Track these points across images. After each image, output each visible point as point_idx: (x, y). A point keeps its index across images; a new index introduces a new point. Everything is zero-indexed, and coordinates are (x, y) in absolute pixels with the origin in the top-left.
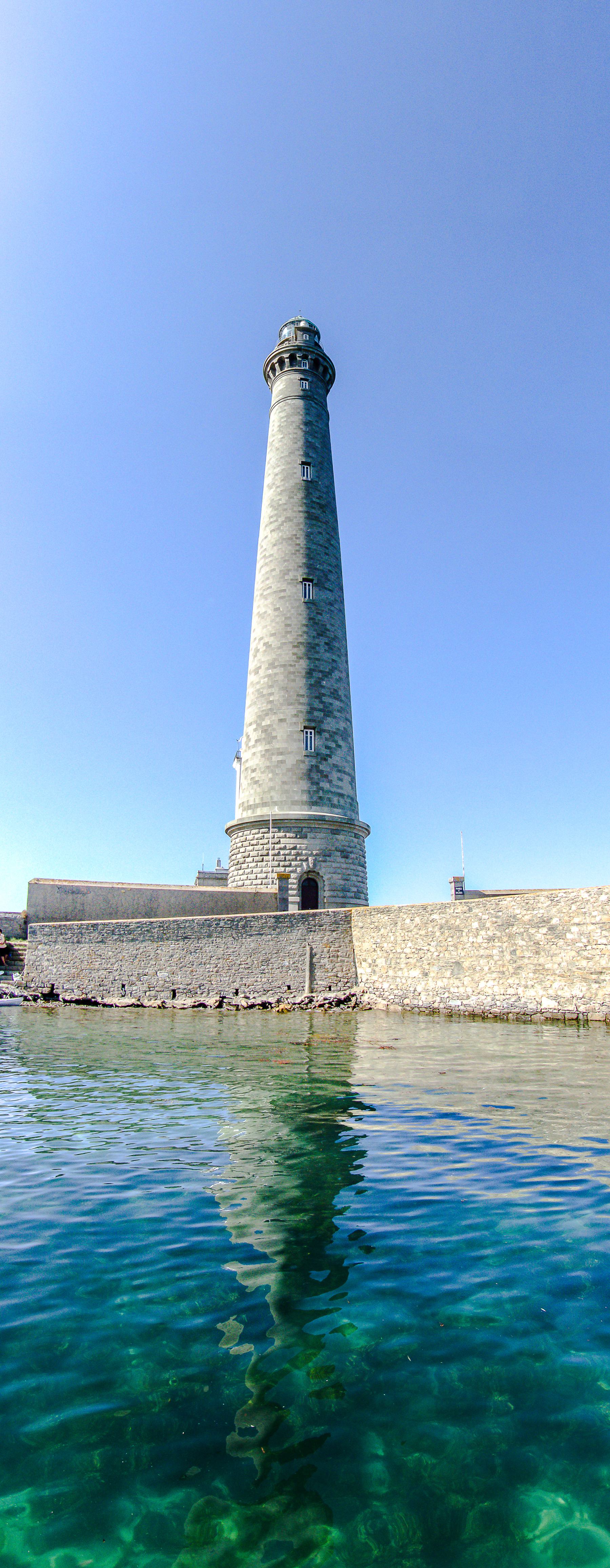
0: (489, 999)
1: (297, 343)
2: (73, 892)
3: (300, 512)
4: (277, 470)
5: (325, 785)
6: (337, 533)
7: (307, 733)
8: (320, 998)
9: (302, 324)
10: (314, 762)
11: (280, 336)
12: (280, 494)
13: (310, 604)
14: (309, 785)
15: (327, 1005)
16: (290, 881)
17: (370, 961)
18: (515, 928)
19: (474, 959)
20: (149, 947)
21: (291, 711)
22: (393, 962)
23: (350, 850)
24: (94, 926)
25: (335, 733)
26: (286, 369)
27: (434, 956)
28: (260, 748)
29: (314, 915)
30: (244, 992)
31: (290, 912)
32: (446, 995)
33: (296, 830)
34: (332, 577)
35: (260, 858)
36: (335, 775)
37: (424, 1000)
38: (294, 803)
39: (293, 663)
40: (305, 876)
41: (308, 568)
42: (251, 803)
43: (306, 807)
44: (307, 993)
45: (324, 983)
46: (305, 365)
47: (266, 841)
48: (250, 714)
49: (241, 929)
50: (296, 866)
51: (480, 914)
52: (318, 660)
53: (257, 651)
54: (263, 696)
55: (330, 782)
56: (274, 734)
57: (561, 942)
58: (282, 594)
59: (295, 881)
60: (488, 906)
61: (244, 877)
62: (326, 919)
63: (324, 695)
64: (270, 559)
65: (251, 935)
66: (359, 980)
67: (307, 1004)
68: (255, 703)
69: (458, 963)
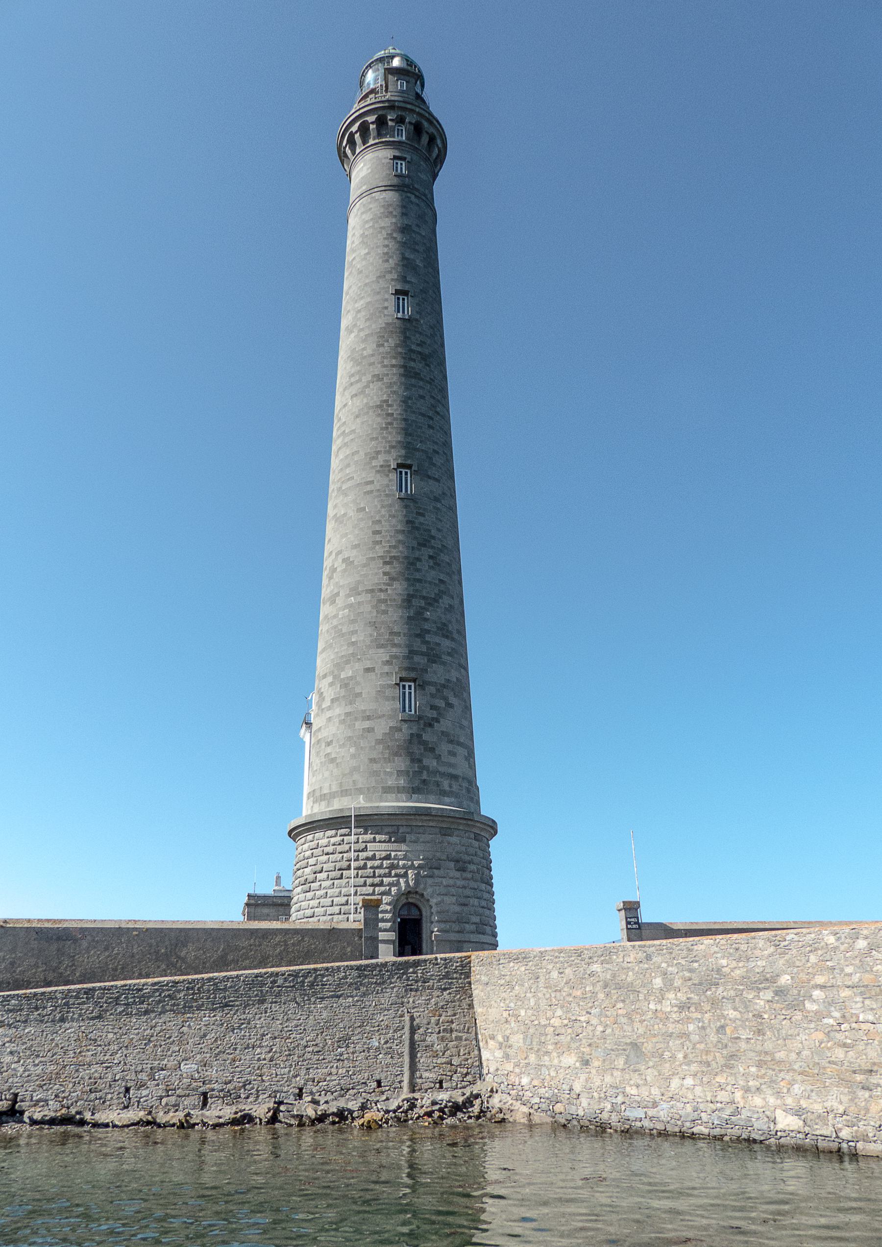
0: (689, 1108)
1: (388, 96)
2: (59, 939)
3: (393, 366)
4: (360, 304)
5: (431, 763)
6: (445, 397)
7: (404, 687)
8: (427, 1102)
9: (396, 62)
10: (414, 730)
11: (361, 84)
12: (364, 341)
13: (408, 501)
14: (408, 763)
15: (436, 1114)
16: (383, 907)
17: (500, 1038)
18: (721, 989)
19: (660, 1038)
20: (169, 1022)
21: (383, 655)
22: (535, 1040)
23: (467, 858)
24: (88, 992)
25: (444, 686)
26: (371, 142)
27: (598, 1033)
28: (338, 711)
29: (416, 964)
30: (312, 1093)
31: (381, 960)
32: (620, 1099)
33: (390, 829)
34: (438, 460)
35: (337, 874)
36: (444, 748)
37: (584, 1108)
38: (387, 790)
39: (384, 587)
40: (403, 900)
41: (405, 448)
42: (325, 791)
43: (404, 796)
44: (405, 1094)
45: (432, 1075)
46: (400, 133)
47: (347, 847)
48: (323, 662)
49: (307, 988)
50: (391, 885)
51: (664, 965)
52: (420, 581)
53: (333, 570)
54: (343, 635)
55: (438, 758)
56: (358, 690)
57: (798, 1016)
58: (369, 488)
59: (389, 908)
60: (676, 952)
61: (314, 903)
62: (433, 971)
63: (428, 632)
64: (352, 437)
65: (323, 998)
66: (485, 1071)
67: (406, 1112)
68: (331, 646)
69: (635, 1046)
